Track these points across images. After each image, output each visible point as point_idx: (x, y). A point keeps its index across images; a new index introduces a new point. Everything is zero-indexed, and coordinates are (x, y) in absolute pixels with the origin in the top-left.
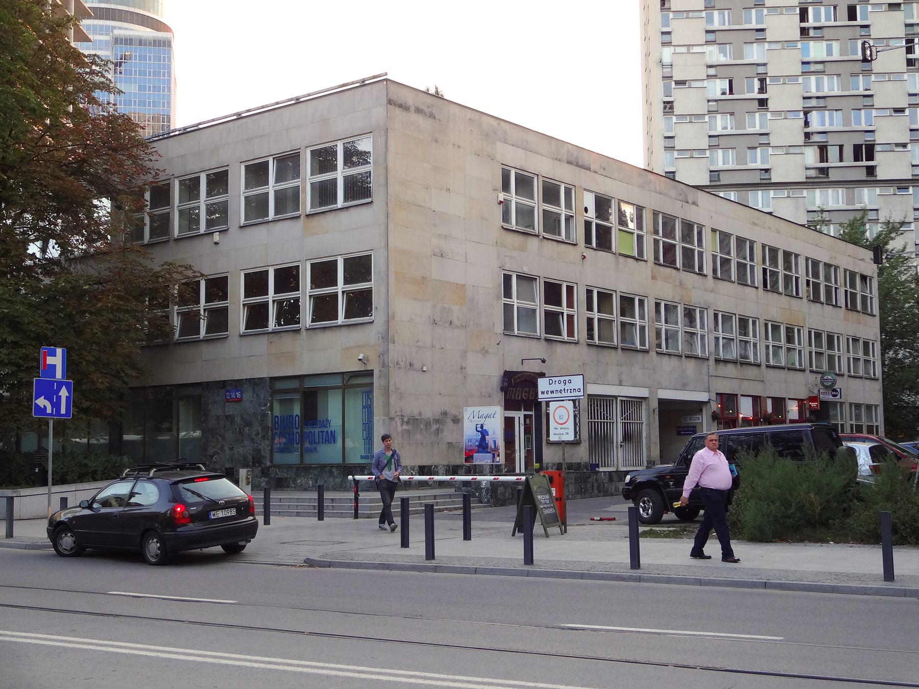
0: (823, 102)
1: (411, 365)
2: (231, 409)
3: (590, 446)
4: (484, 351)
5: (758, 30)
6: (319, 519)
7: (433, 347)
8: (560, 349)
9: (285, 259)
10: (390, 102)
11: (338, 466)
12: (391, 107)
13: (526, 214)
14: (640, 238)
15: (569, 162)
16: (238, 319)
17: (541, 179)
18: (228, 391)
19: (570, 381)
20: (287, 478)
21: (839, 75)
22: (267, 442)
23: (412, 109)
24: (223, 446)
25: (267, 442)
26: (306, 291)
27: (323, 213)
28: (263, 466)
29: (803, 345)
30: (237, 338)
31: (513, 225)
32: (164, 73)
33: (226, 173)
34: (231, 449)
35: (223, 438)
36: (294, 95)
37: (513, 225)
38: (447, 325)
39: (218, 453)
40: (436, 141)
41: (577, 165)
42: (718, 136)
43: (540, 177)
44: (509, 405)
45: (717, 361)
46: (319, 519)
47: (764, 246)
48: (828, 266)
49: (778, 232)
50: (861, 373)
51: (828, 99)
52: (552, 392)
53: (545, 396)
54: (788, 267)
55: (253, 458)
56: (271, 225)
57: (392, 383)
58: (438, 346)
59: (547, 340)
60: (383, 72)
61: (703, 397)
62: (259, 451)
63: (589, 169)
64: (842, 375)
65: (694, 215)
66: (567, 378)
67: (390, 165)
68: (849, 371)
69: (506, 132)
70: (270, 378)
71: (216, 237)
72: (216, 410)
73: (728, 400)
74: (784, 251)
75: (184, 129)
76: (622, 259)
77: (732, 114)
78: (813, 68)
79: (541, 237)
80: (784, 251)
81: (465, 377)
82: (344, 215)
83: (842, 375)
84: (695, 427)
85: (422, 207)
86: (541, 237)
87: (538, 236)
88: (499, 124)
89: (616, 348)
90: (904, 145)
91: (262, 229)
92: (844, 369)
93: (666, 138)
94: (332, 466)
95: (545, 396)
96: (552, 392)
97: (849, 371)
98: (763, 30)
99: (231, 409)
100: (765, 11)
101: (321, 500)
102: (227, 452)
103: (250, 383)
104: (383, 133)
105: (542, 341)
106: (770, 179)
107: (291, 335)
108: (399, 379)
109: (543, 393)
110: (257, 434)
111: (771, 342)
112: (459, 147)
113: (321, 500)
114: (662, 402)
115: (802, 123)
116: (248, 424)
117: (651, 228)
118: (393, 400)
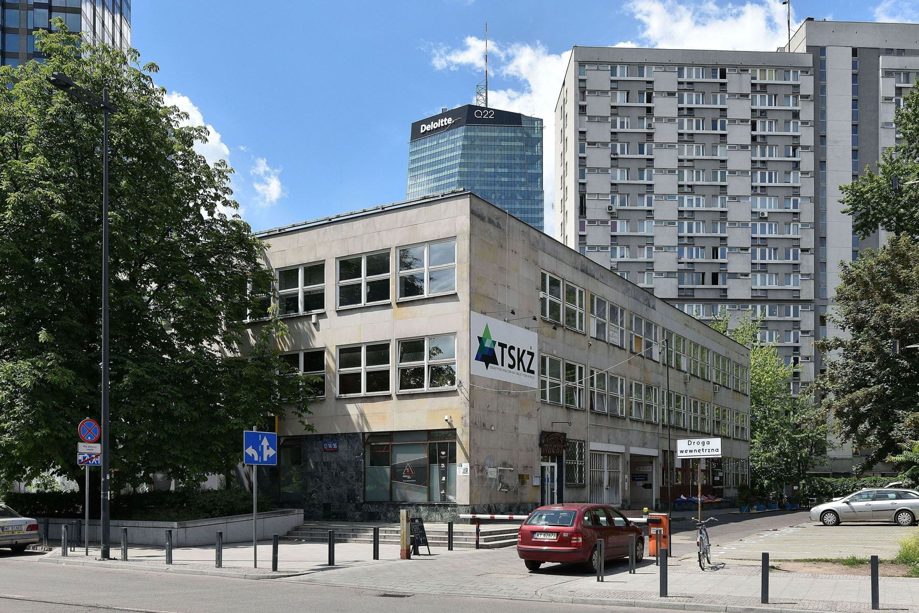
1: (484, 425)
2: (328, 457)
4: (529, 416)
8: (575, 415)
13: (555, 307)
14: (622, 331)
15: (582, 271)
18: (326, 442)
19: (708, 443)
20: (378, 513)
22: (361, 484)
23: (486, 219)
24: (321, 486)
25: (361, 484)
28: (357, 502)
33: (323, 265)
34: (328, 489)
35: (321, 479)
36: (380, 206)
38: (506, 394)
39: (317, 492)
40: (502, 247)
41: (587, 274)
44: (546, 456)
49: (699, 332)
55: (348, 496)
58: (501, 411)
59: (567, 408)
61: (654, 452)
62: (354, 490)
63: (593, 277)
69: (544, 243)
75: (280, 230)
76: (611, 347)
77: (628, 247)
79: (564, 328)
81: (517, 436)
84: (647, 475)
85: (492, 299)
86: (564, 328)
89: (607, 415)
90: (747, 275)
96: (691, 451)
99: (328, 457)
101: (450, 532)
102: (325, 490)
103: (345, 437)
105: (564, 409)
106: (726, 296)
110: (352, 477)
112: (516, 253)
113: (450, 532)
114: (633, 456)
115: (676, 255)
117: (629, 325)
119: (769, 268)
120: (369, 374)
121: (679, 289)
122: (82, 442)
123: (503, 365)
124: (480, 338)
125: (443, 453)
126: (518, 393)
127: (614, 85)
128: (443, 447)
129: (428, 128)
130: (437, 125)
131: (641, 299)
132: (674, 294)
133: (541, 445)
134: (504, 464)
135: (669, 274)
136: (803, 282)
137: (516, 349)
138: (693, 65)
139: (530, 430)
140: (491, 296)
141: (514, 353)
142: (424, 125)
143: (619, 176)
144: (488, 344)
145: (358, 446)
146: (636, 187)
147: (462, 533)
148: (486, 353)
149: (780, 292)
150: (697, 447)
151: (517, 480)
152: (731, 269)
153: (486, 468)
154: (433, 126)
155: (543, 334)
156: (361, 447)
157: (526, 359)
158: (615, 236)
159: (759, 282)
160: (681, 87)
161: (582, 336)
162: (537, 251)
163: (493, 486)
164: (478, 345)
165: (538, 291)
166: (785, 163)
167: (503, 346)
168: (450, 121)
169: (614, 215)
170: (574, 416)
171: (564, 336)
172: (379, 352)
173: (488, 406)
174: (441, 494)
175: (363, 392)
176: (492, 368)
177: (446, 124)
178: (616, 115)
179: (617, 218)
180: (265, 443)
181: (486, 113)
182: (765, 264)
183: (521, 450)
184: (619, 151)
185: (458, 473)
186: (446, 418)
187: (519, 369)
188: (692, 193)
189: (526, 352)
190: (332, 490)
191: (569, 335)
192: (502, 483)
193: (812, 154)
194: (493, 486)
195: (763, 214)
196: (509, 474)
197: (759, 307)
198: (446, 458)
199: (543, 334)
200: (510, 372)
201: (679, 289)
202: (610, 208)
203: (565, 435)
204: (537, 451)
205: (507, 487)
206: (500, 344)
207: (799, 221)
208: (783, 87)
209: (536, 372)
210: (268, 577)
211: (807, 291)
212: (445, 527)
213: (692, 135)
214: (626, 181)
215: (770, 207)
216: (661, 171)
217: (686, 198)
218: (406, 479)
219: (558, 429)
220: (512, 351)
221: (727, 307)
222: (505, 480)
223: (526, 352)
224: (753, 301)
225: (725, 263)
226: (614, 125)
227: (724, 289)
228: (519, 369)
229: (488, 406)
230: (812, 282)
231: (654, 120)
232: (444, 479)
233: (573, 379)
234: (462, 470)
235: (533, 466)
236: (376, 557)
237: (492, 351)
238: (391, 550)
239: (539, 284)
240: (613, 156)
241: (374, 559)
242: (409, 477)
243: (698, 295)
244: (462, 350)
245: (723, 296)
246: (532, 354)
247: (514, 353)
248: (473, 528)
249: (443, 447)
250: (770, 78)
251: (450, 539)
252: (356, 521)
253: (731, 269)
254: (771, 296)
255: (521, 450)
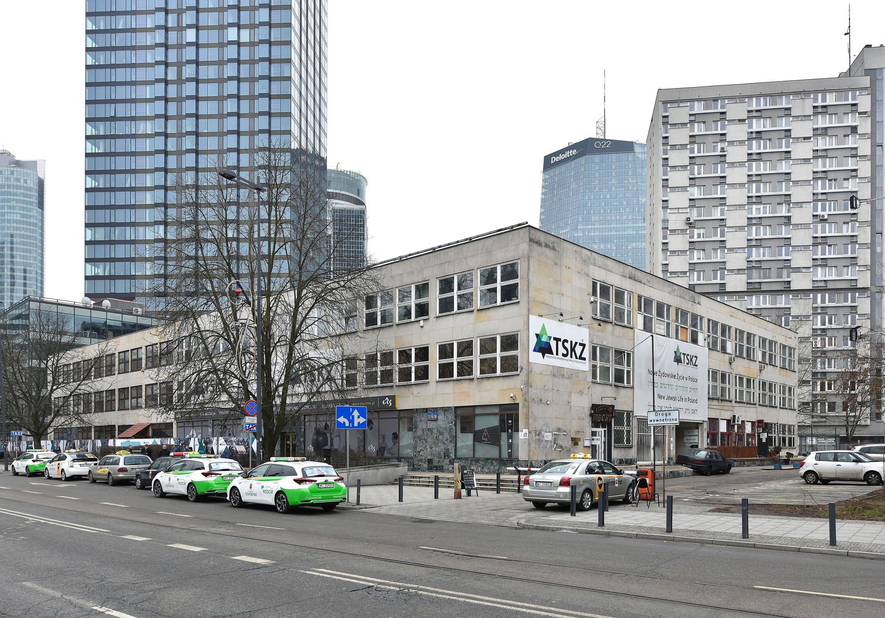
0: (759, 243)
1: (541, 400)
2: (431, 425)
3: (638, 448)
5: (721, 198)
6: (497, 493)
7: (553, 389)
9: (464, 336)
10: (531, 240)
11: (496, 460)
12: (532, 244)
14: (668, 324)
15: (630, 278)
16: (434, 372)
17: (614, 288)
21: (770, 226)
22: (453, 445)
23: (543, 244)
24: (426, 446)
26: (476, 358)
27: (488, 308)
28: (450, 458)
29: (756, 390)
30: (435, 383)
31: (598, 316)
32: (361, 229)
33: (427, 284)
35: (426, 442)
37: (598, 316)
40: (556, 264)
41: (635, 280)
42: (695, 263)
43: (614, 287)
44: (595, 424)
45: (736, 402)
46: (497, 493)
47: (736, 330)
48: (771, 342)
49: (745, 321)
50: (767, 403)
51: (763, 241)
52: (657, 421)
53: (653, 423)
54: (748, 342)
55: (444, 454)
56: (455, 316)
57: (530, 410)
58: (556, 389)
59: (615, 386)
60: (525, 221)
63: (641, 282)
64: (776, 407)
65: (700, 310)
66: (668, 412)
67: (531, 279)
68: (780, 405)
69: (595, 259)
70: (455, 407)
71: (422, 323)
72: (422, 425)
73: (713, 422)
74: (747, 333)
78: (754, 222)
80: (747, 333)
81: (570, 408)
82: (501, 310)
83: (776, 407)
87: (612, 323)
88: (591, 254)
91: (450, 319)
92: (778, 404)
93: (663, 264)
94: (493, 459)
95: (653, 423)
96: (657, 421)
97: (780, 405)
98: (724, 198)
100: (726, 187)
102: (429, 449)
104: (526, 259)
106: (790, 287)
107: (468, 382)
108: (536, 409)
109: (651, 421)
111: (738, 388)
112: (569, 268)
116: (441, 434)
118: (530, 421)
119: (829, 263)
120: (502, 358)
121: (748, 283)
122: (247, 416)
123: (557, 354)
124: (537, 335)
125: (510, 422)
126: (573, 374)
127: (693, 118)
128: (510, 417)
129: (556, 159)
130: (565, 156)
131: (687, 297)
132: (744, 288)
133: (591, 415)
134: (559, 430)
135: (740, 271)
136: (861, 272)
137: (569, 342)
138: (761, 95)
139: (583, 404)
140: (547, 302)
141: (568, 345)
142: (554, 157)
143: (695, 192)
144: (544, 339)
145: (451, 416)
146: (711, 200)
147: (506, 481)
148: (543, 346)
149: (839, 282)
150: (661, 417)
151: (570, 442)
152: (794, 264)
153: (543, 433)
154: (561, 157)
155: (593, 329)
156: (453, 418)
157: (578, 349)
158: (693, 242)
159: (820, 274)
160: (751, 115)
161: (630, 329)
162: (588, 266)
163: (548, 446)
164: (536, 340)
165: (589, 297)
166: (844, 172)
167: (557, 340)
168: (574, 152)
169: (690, 224)
170: (622, 392)
171: (613, 330)
172: (466, 347)
173: (545, 386)
174: (508, 452)
175: (498, 373)
176: (547, 357)
177: (571, 155)
178: (694, 142)
179: (694, 227)
180: (356, 413)
181: (604, 143)
182: (825, 259)
183: (574, 419)
184: (696, 172)
185: (520, 437)
186: (512, 395)
187: (571, 357)
188: (760, 203)
189: (578, 344)
190: (434, 449)
191: (618, 329)
192: (557, 445)
193: (869, 162)
194: (548, 446)
195: (823, 216)
196: (562, 437)
197: (819, 296)
198: (512, 425)
199: (593, 329)
200: (564, 359)
201: (748, 283)
202: (688, 219)
203: (613, 406)
204: (588, 421)
205: (561, 447)
206: (555, 339)
207: (856, 221)
208: (842, 107)
209: (587, 359)
210: (821, 553)
211: (864, 280)
212: (495, 477)
213: (759, 154)
214: (702, 197)
215: (830, 210)
216: (732, 185)
217: (754, 207)
218: (484, 441)
219: (607, 402)
220: (566, 344)
221: (791, 297)
222: (560, 442)
223: (578, 344)
224: (815, 290)
225: (789, 260)
226: (692, 151)
227: (788, 281)
228: (571, 357)
229: (545, 386)
230: (869, 272)
231: (726, 145)
232: (510, 441)
233: (621, 364)
234: (523, 435)
235: (584, 431)
236: (436, 497)
237: (548, 344)
238: (446, 493)
239: (591, 291)
240: (691, 177)
241: (435, 498)
242: (486, 440)
243: (764, 287)
244: (523, 344)
245: (787, 287)
246: (584, 345)
247: (568, 345)
248: (516, 477)
249: (510, 417)
250: (831, 99)
251: (498, 485)
252: (449, 472)
253: (794, 264)
254: (830, 286)
255: (574, 419)
